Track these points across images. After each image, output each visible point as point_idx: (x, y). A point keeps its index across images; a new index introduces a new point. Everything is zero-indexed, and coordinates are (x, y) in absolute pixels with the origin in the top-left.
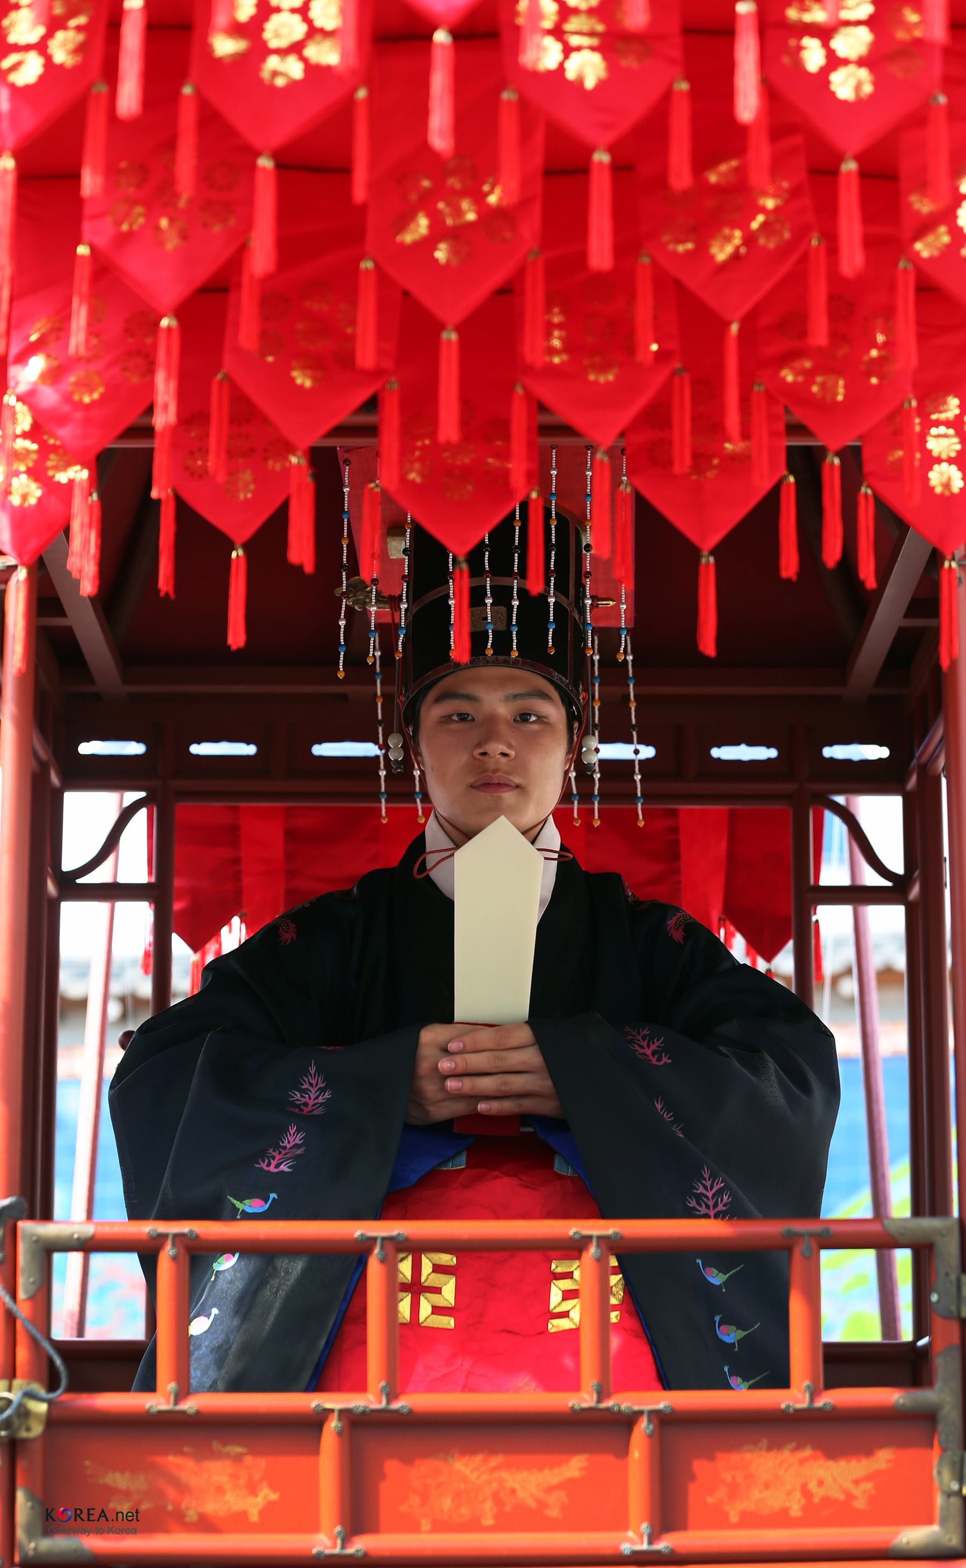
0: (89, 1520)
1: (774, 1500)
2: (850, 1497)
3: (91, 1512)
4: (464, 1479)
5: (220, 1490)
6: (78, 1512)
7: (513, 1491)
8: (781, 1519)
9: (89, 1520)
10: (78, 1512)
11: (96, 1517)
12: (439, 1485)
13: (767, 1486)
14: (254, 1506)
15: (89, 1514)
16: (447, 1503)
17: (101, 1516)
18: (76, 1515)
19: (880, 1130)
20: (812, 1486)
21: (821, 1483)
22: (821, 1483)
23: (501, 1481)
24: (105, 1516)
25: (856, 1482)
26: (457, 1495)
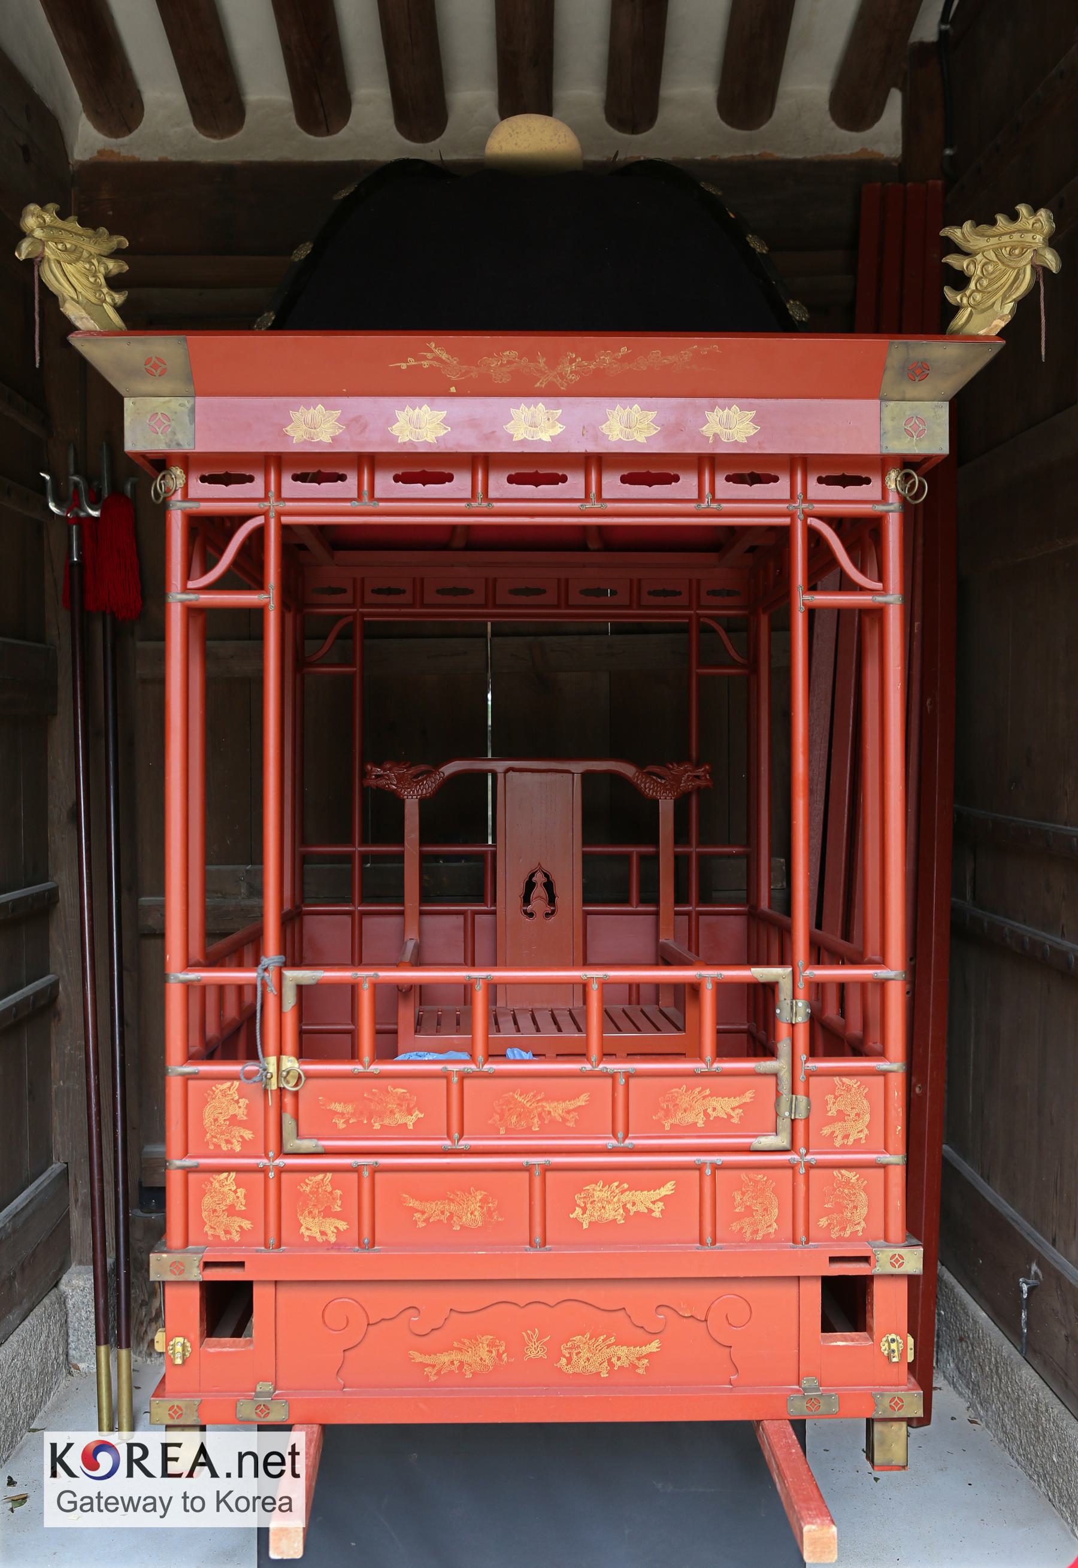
0: (165, 1474)
1: (689, 1118)
2: (730, 1116)
3: (172, 1452)
4: (523, 1106)
5: (392, 1112)
6: (137, 1453)
7: (549, 1112)
8: (691, 1129)
9: (165, 1474)
10: (137, 1453)
11: (182, 1465)
12: (510, 1109)
13: (685, 1111)
14: (410, 1121)
15: (166, 1459)
16: (514, 1119)
17: (196, 1463)
18: (130, 1460)
19: (864, 867)
20: (710, 1111)
21: (714, 1109)
22: (714, 1109)
23: (543, 1107)
24: (208, 1463)
25: (733, 1109)
26: (520, 1115)
